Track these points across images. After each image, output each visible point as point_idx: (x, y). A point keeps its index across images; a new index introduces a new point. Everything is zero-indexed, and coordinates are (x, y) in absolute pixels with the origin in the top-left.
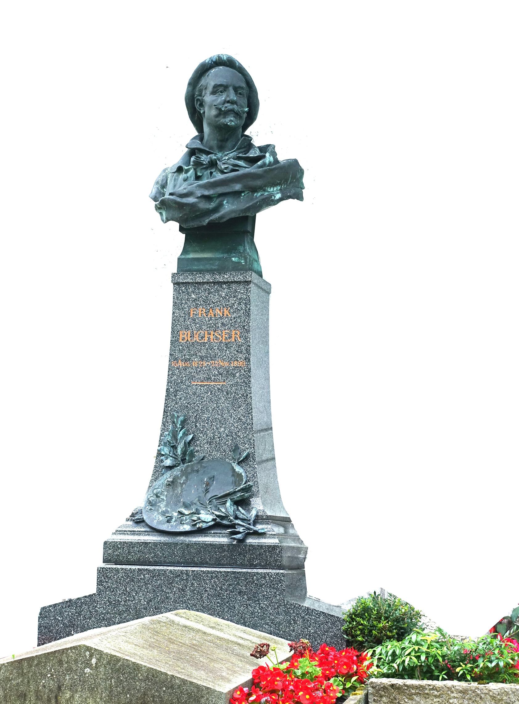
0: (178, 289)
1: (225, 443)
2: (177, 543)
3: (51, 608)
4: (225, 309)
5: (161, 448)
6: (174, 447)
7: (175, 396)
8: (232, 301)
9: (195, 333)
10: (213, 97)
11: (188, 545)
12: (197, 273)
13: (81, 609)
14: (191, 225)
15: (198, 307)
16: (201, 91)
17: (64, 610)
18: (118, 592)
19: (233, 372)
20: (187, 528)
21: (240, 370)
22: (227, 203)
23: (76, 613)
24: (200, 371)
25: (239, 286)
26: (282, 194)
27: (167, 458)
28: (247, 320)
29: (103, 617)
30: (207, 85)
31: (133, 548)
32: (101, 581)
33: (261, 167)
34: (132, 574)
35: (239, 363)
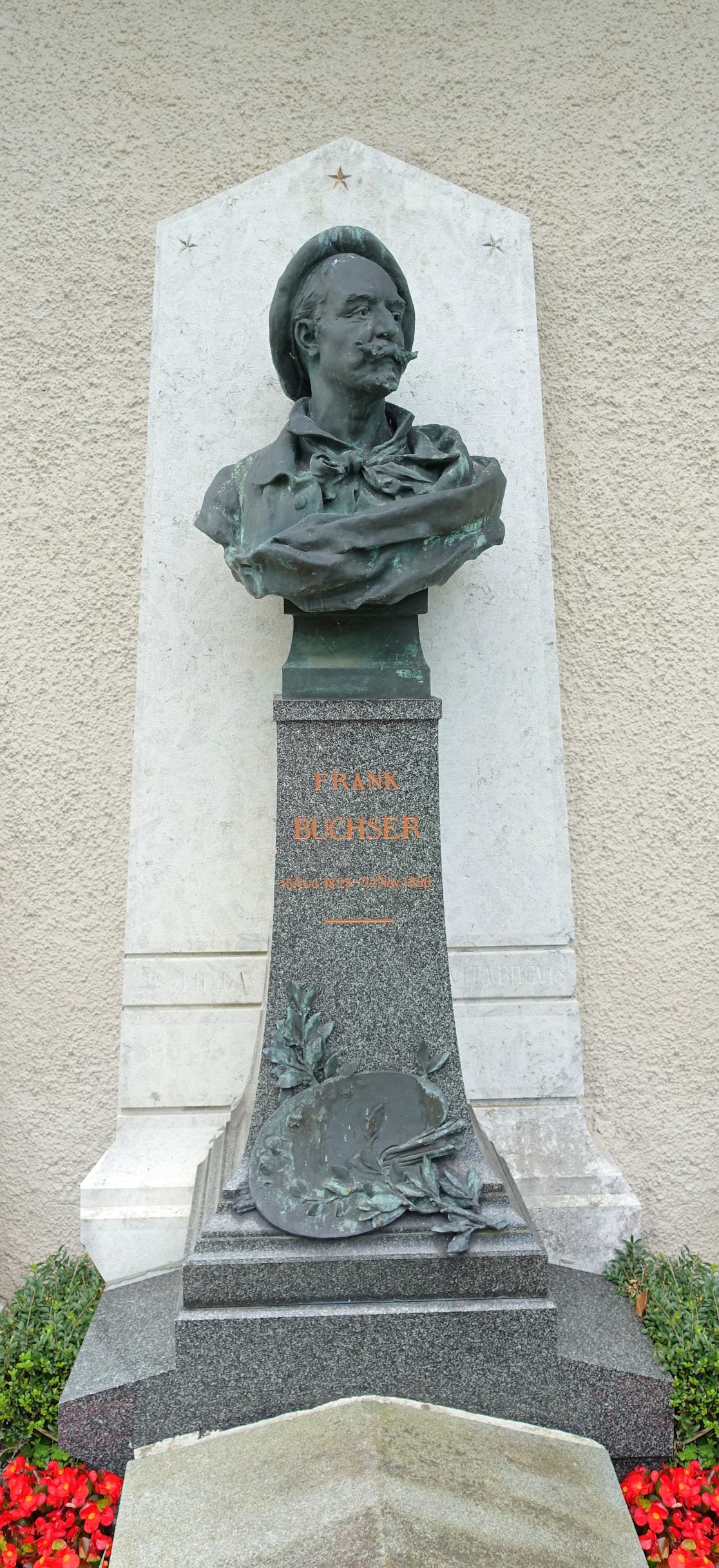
1: (398, 1037)
2: (336, 1262)
3: (80, 1404)
4: (387, 774)
5: (270, 1052)
6: (298, 1050)
7: (292, 946)
8: (401, 757)
9: (326, 822)
10: (343, 324)
11: (359, 1264)
13: (144, 1401)
14: (322, 607)
17: (109, 1405)
18: (222, 1364)
20: (351, 1227)
21: (422, 895)
22: (401, 562)
23: (135, 1409)
24: (340, 898)
26: (487, 535)
27: (284, 1070)
29: (194, 1413)
30: (327, 293)
31: (245, 1275)
32: (184, 1346)
33: (453, 483)
34: (248, 1330)
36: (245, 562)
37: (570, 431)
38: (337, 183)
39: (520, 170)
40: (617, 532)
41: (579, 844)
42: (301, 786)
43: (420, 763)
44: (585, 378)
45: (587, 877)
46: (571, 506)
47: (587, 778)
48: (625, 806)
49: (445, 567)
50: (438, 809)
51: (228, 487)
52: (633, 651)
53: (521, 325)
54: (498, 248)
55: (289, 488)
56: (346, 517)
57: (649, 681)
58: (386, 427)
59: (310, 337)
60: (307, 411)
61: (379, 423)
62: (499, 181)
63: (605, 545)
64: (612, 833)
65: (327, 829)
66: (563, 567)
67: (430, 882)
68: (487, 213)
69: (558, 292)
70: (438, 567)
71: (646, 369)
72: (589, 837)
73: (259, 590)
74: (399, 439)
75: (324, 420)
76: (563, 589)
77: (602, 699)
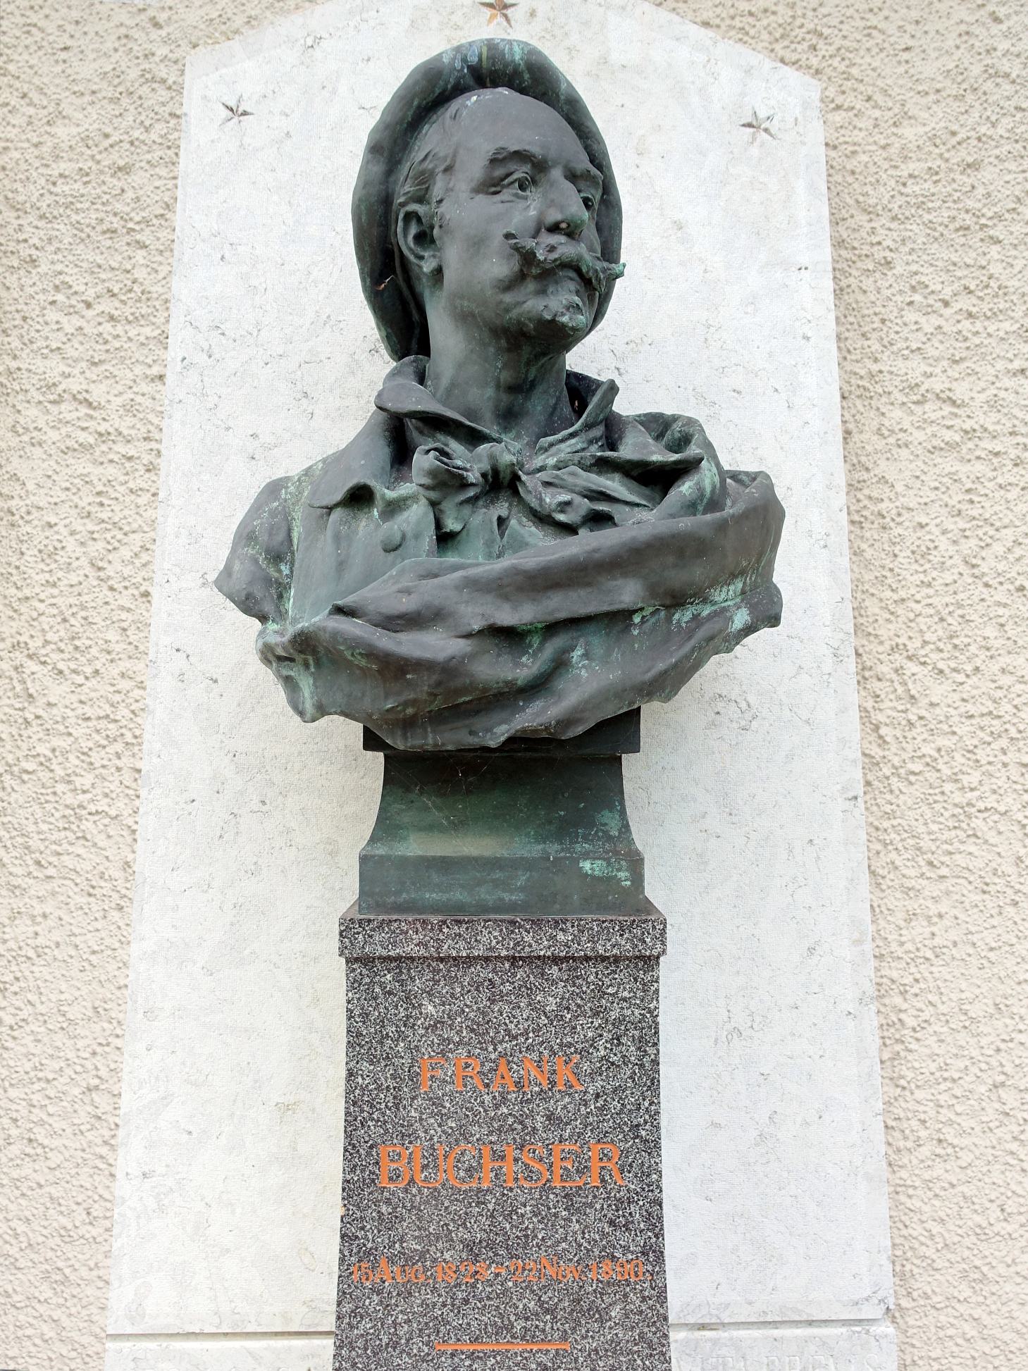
0: (367, 980)
4: (559, 1062)
9: (440, 1153)
12: (444, 922)
14: (430, 741)
15: (451, 1051)
16: (424, 180)
19: (599, 1301)
21: (626, 1296)
22: (586, 655)
24: (466, 1301)
25: (615, 972)
26: (752, 608)
28: (646, 1104)
33: (691, 507)
35: (618, 1269)
36: (280, 652)
37: (880, 444)
38: (492, 17)
39: (799, 22)
40: (960, 612)
41: (897, 1134)
42: (392, 1083)
43: (624, 1040)
44: (906, 358)
45: (911, 1191)
46: (883, 567)
47: (910, 1022)
48: (974, 1070)
49: (675, 666)
50: (658, 1128)
51: (273, 514)
52: (986, 809)
53: (804, 260)
54: (766, 130)
55: (376, 513)
56: (478, 565)
57: (1012, 859)
58: (567, 410)
59: (425, 238)
60: (421, 379)
61: (552, 402)
62: (765, 36)
63: (940, 633)
64: (953, 1117)
65: (443, 1166)
66: (871, 668)
67: (642, 1269)
68: (748, 71)
69: (862, 218)
70: (661, 666)
71: (1006, 347)
72: (914, 1123)
73: (309, 706)
74: (588, 426)
75: (449, 391)
76: (869, 704)
77: (935, 889)
